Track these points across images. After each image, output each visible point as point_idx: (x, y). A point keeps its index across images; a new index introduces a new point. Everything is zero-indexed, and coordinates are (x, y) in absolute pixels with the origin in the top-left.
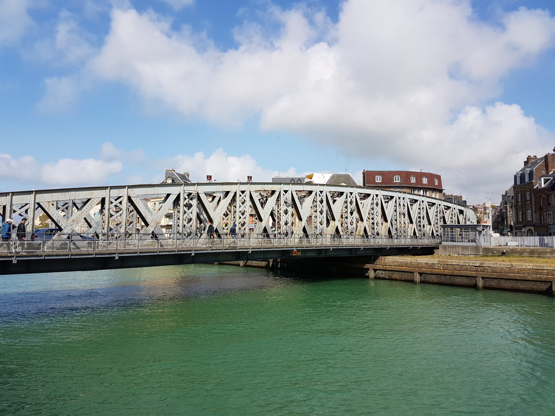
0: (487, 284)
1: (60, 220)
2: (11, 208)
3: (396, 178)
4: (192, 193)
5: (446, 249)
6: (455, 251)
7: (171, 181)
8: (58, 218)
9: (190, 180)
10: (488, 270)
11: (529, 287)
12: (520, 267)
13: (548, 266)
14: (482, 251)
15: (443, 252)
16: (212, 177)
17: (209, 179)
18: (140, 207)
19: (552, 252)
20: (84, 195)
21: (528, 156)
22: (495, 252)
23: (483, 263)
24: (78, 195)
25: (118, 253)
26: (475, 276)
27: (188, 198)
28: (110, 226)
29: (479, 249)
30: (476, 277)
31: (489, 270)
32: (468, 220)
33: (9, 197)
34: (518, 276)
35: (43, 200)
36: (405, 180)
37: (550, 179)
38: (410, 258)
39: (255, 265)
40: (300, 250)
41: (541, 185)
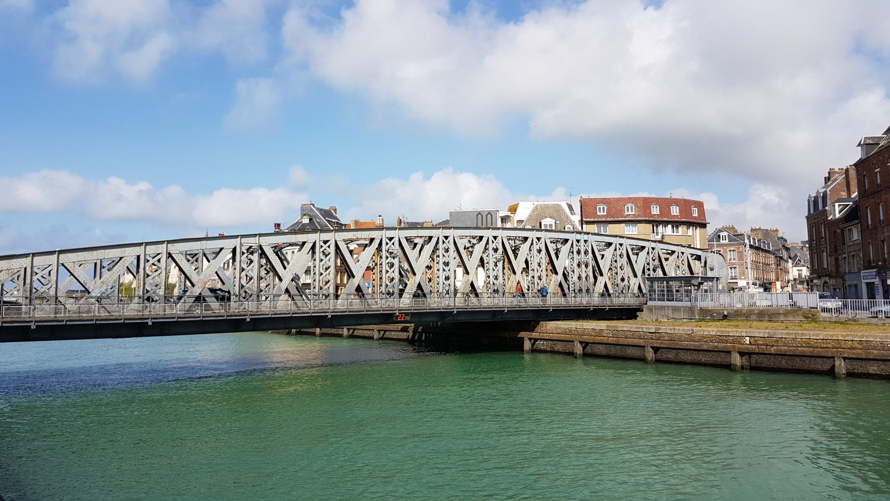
0: (664, 357)
1: (88, 282)
2: (101, 265)
3: (628, 207)
4: (252, 246)
5: (652, 311)
6: (663, 313)
7: (308, 219)
8: (85, 280)
9: (339, 218)
10: (664, 337)
11: (712, 360)
12: (702, 333)
13: (733, 331)
14: (698, 313)
15: (648, 315)
16: (281, 225)
17: (276, 227)
18: (184, 265)
19: (787, 313)
20: (115, 253)
21: (830, 169)
22: (715, 314)
23: (659, 329)
24: (108, 254)
25: (152, 318)
26: (643, 345)
27: (248, 252)
28: (146, 288)
29: (694, 311)
30: (644, 347)
31: (666, 338)
32: (711, 270)
33: (30, 258)
34: (693, 345)
35: (67, 261)
36: (642, 211)
37: (849, 204)
38: (576, 323)
39: (394, 337)
40: (408, 313)
41: (835, 215)
